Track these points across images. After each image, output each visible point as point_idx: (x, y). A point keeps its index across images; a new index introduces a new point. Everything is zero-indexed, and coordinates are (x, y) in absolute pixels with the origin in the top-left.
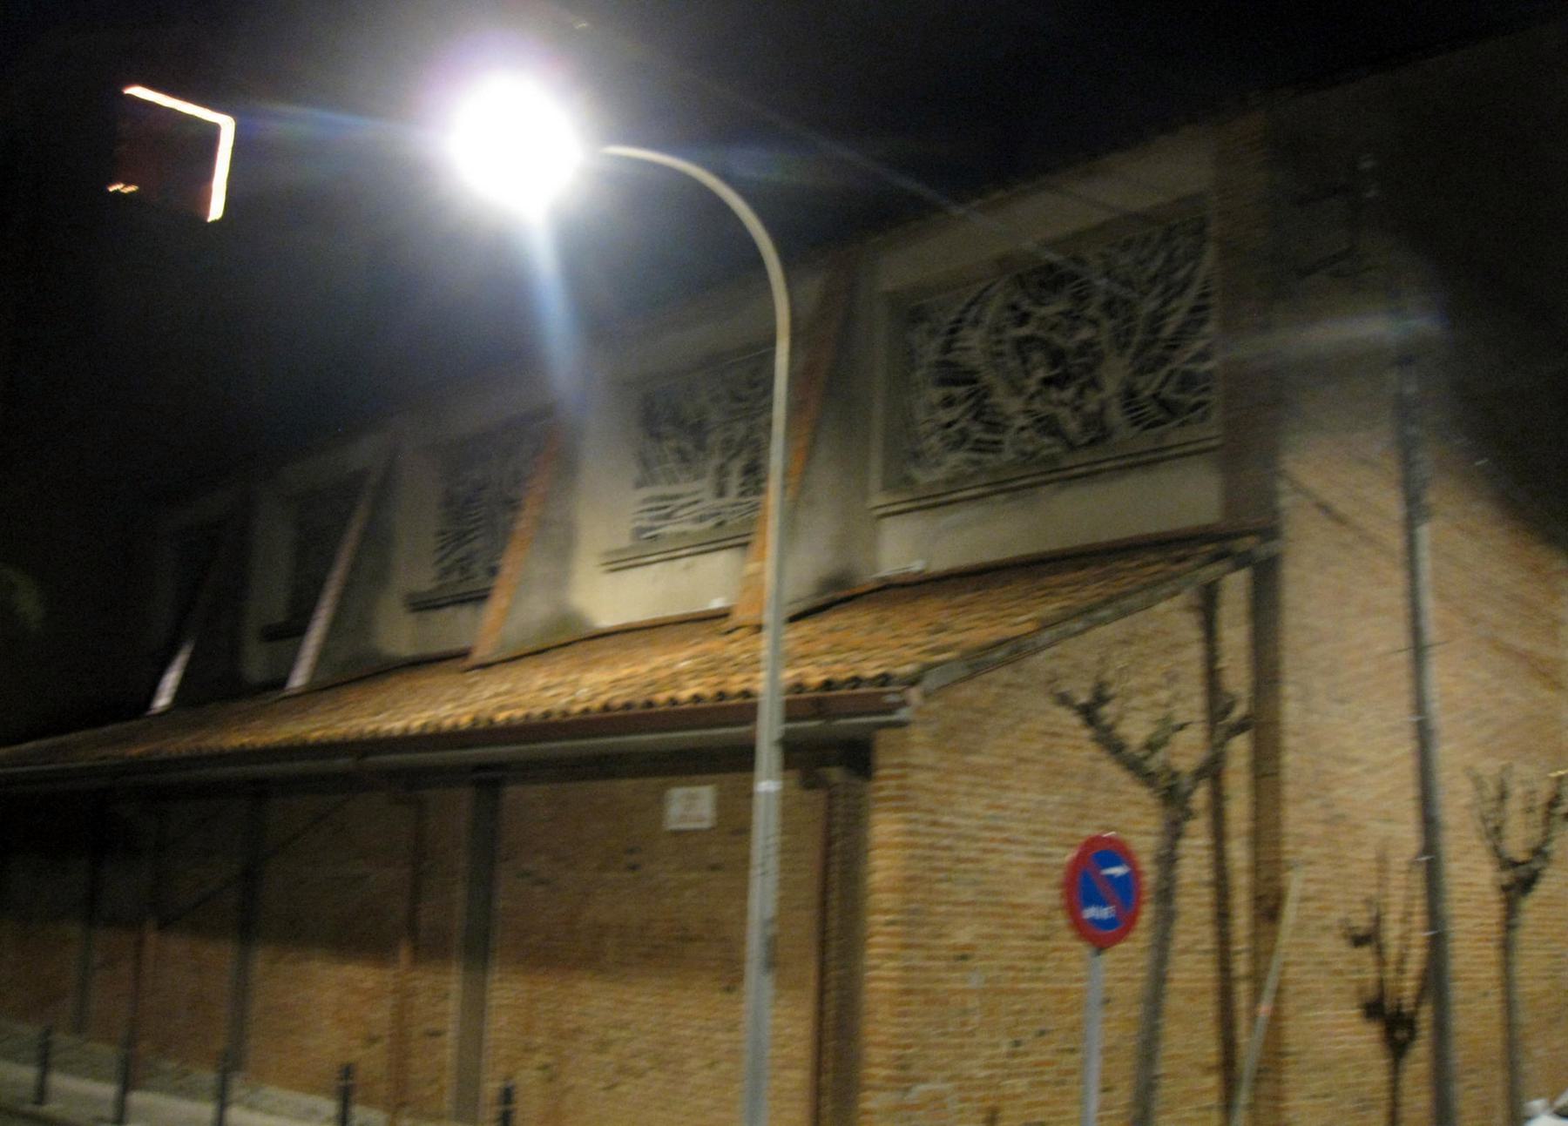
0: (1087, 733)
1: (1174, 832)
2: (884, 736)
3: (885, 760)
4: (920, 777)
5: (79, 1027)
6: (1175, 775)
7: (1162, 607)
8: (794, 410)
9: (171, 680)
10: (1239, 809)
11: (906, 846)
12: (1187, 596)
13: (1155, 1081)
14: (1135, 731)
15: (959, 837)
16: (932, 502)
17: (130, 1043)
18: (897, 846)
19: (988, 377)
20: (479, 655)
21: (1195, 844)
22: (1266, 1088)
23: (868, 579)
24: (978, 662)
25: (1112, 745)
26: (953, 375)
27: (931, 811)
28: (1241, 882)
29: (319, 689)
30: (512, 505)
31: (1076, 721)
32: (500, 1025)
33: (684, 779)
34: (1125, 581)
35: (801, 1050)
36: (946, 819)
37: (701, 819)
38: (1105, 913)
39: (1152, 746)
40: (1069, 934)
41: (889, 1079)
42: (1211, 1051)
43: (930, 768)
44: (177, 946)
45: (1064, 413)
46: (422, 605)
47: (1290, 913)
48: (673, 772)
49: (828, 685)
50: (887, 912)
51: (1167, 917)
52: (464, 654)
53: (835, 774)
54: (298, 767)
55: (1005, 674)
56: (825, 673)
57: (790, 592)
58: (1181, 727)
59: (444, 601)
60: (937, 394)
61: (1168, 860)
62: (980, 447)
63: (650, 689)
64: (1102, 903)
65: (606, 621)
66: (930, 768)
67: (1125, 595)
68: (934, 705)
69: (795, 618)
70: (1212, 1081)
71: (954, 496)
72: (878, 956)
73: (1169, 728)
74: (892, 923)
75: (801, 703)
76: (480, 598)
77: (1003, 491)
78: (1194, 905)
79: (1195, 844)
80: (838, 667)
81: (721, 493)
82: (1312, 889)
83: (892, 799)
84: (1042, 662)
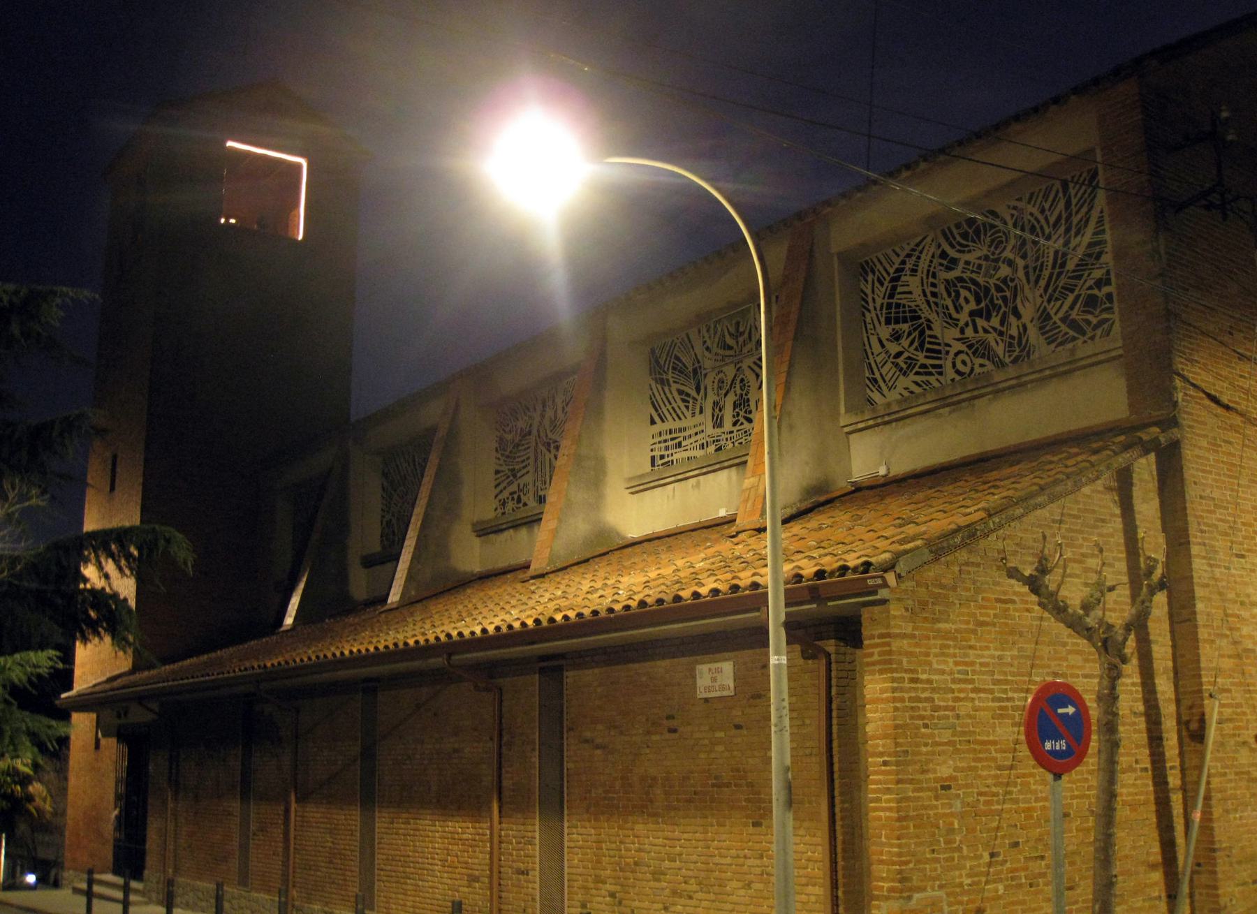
0: (1034, 598)
1: (1113, 675)
2: (866, 614)
3: (869, 631)
4: (896, 644)
5: (244, 880)
6: (1110, 627)
7: (1086, 490)
8: (774, 351)
9: (295, 601)
10: (1162, 651)
11: (894, 700)
12: (1107, 479)
13: (1114, 880)
14: (1074, 594)
15: (934, 690)
16: (887, 419)
17: (283, 892)
18: (887, 700)
19: (926, 313)
20: (535, 568)
21: (1130, 679)
22: (1204, 879)
23: (842, 485)
24: (939, 548)
25: (1059, 610)
26: (897, 314)
27: (912, 671)
28: (1168, 710)
29: (408, 603)
30: (553, 446)
31: (1026, 589)
32: (574, 861)
33: (707, 657)
34: (927, 248)
35: (819, 871)
36: (924, 677)
37: (722, 688)
38: (1061, 745)
39: (1086, 607)
40: (1033, 762)
41: (891, 890)
42: (1155, 851)
43: (904, 636)
44: (314, 813)
45: (991, 338)
46: (485, 530)
47: (1212, 734)
48: (693, 653)
49: (820, 574)
50: (881, 754)
51: (1112, 746)
52: (526, 567)
53: (830, 646)
54: (402, 666)
55: (963, 555)
56: (815, 565)
57: (782, 499)
58: (1111, 589)
59: (504, 526)
60: (885, 332)
61: (1109, 698)
62: (925, 370)
63: (677, 586)
64: (1056, 737)
65: (634, 533)
66: (904, 636)
67: (1056, 482)
68: (908, 584)
69: (785, 521)
70: (1157, 876)
71: (909, 412)
72: (875, 791)
73: (1103, 589)
74: (885, 763)
75: (798, 590)
76: (534, 521)
77: (948, 405)
78: (1132, 732)
79: (1130, 679)
80: (828, 558)
81: (718, 423)
82: (1228, 711)
83: (879, 662)
84: (992, 543)
